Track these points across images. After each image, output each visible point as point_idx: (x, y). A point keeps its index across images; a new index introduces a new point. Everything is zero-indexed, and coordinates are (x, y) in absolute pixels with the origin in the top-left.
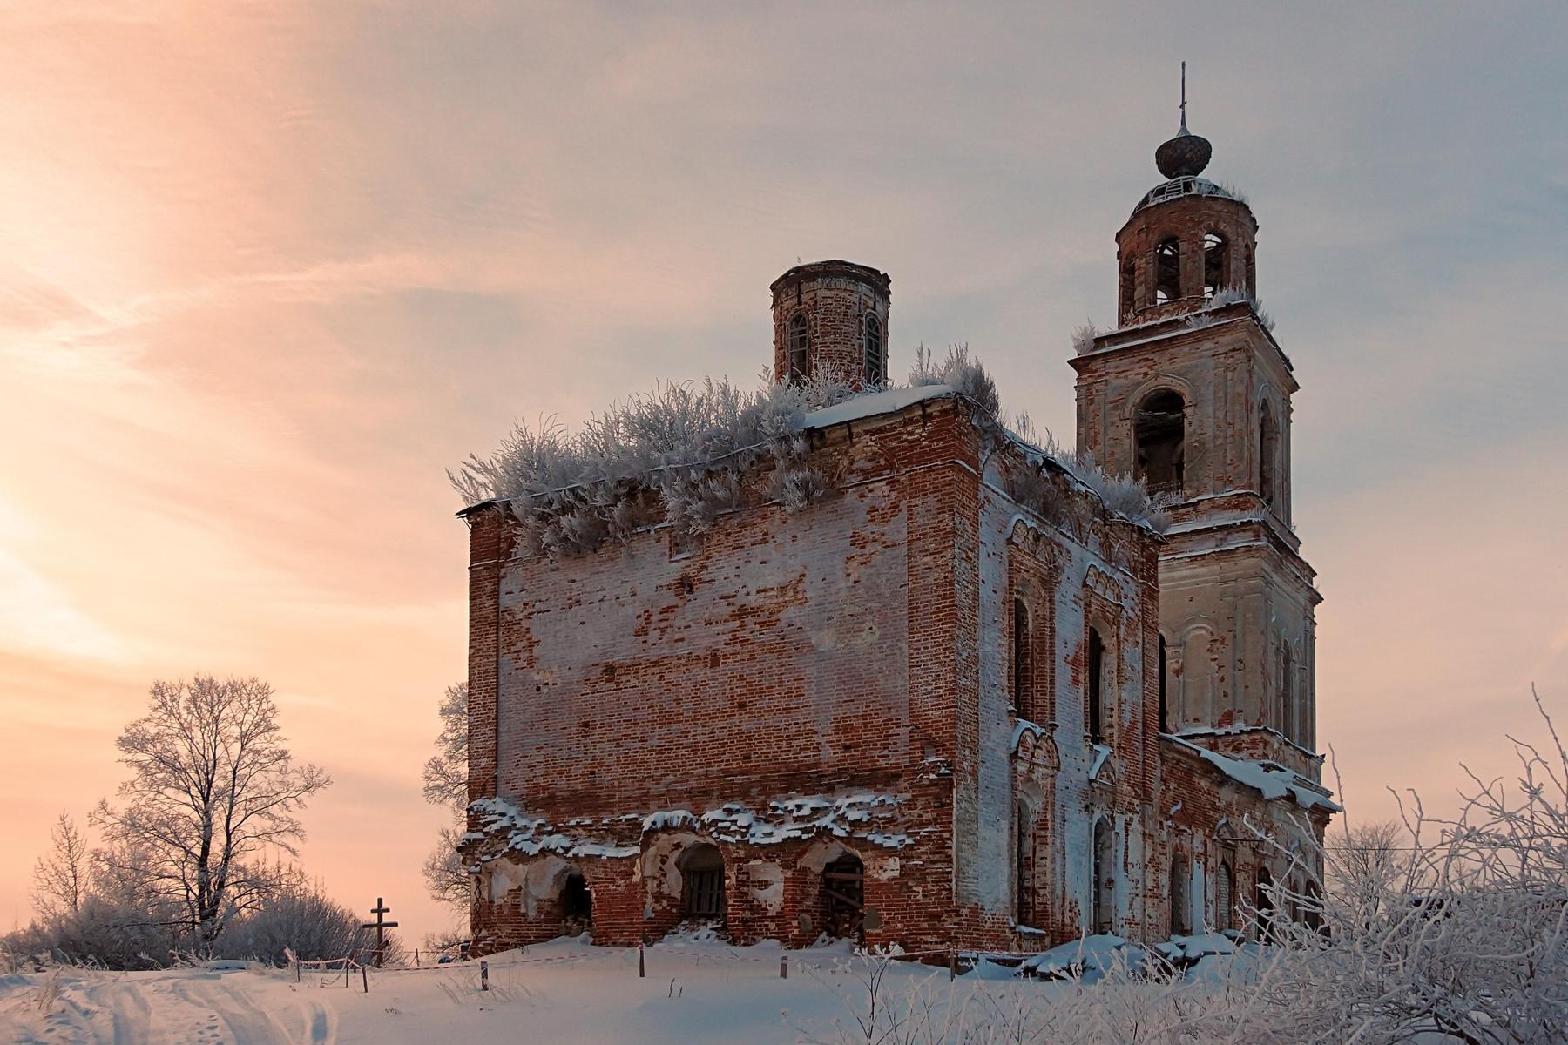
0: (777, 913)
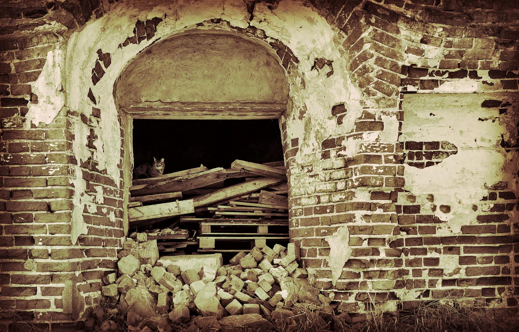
0: (464, 229)
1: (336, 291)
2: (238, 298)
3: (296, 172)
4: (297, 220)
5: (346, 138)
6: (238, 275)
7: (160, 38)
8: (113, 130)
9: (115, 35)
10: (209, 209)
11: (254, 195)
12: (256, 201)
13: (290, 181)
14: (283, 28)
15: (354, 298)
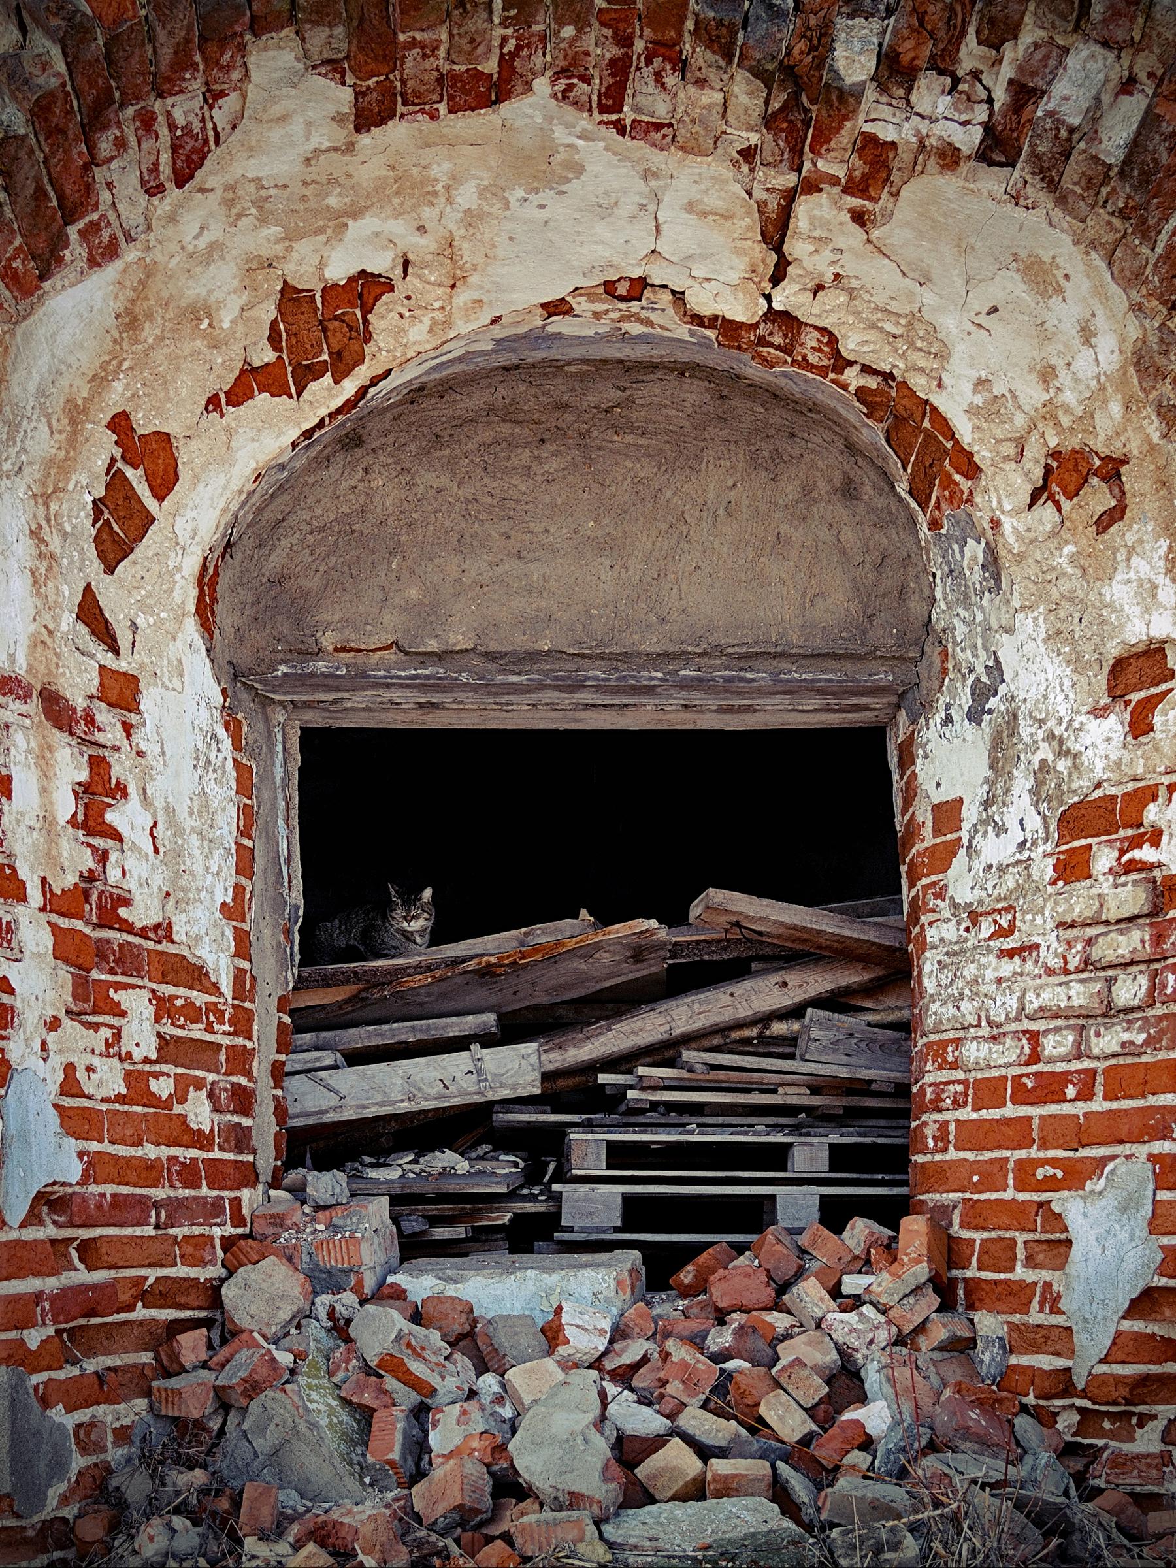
1: (1088, 1404)
2: (690, 1431)
3: (946, 936)
4: (944, 1125)
5: (1162, 791)
6: (697, 1342)
7: (388, 373)
8: (202, 763)
9: (187, 351)
10: (603, 1078)
11: (779, 1028)
12: (787, 1050)
13: (920, 973)
14: (913, 318)
15: (1157, 1436)
